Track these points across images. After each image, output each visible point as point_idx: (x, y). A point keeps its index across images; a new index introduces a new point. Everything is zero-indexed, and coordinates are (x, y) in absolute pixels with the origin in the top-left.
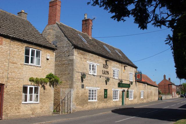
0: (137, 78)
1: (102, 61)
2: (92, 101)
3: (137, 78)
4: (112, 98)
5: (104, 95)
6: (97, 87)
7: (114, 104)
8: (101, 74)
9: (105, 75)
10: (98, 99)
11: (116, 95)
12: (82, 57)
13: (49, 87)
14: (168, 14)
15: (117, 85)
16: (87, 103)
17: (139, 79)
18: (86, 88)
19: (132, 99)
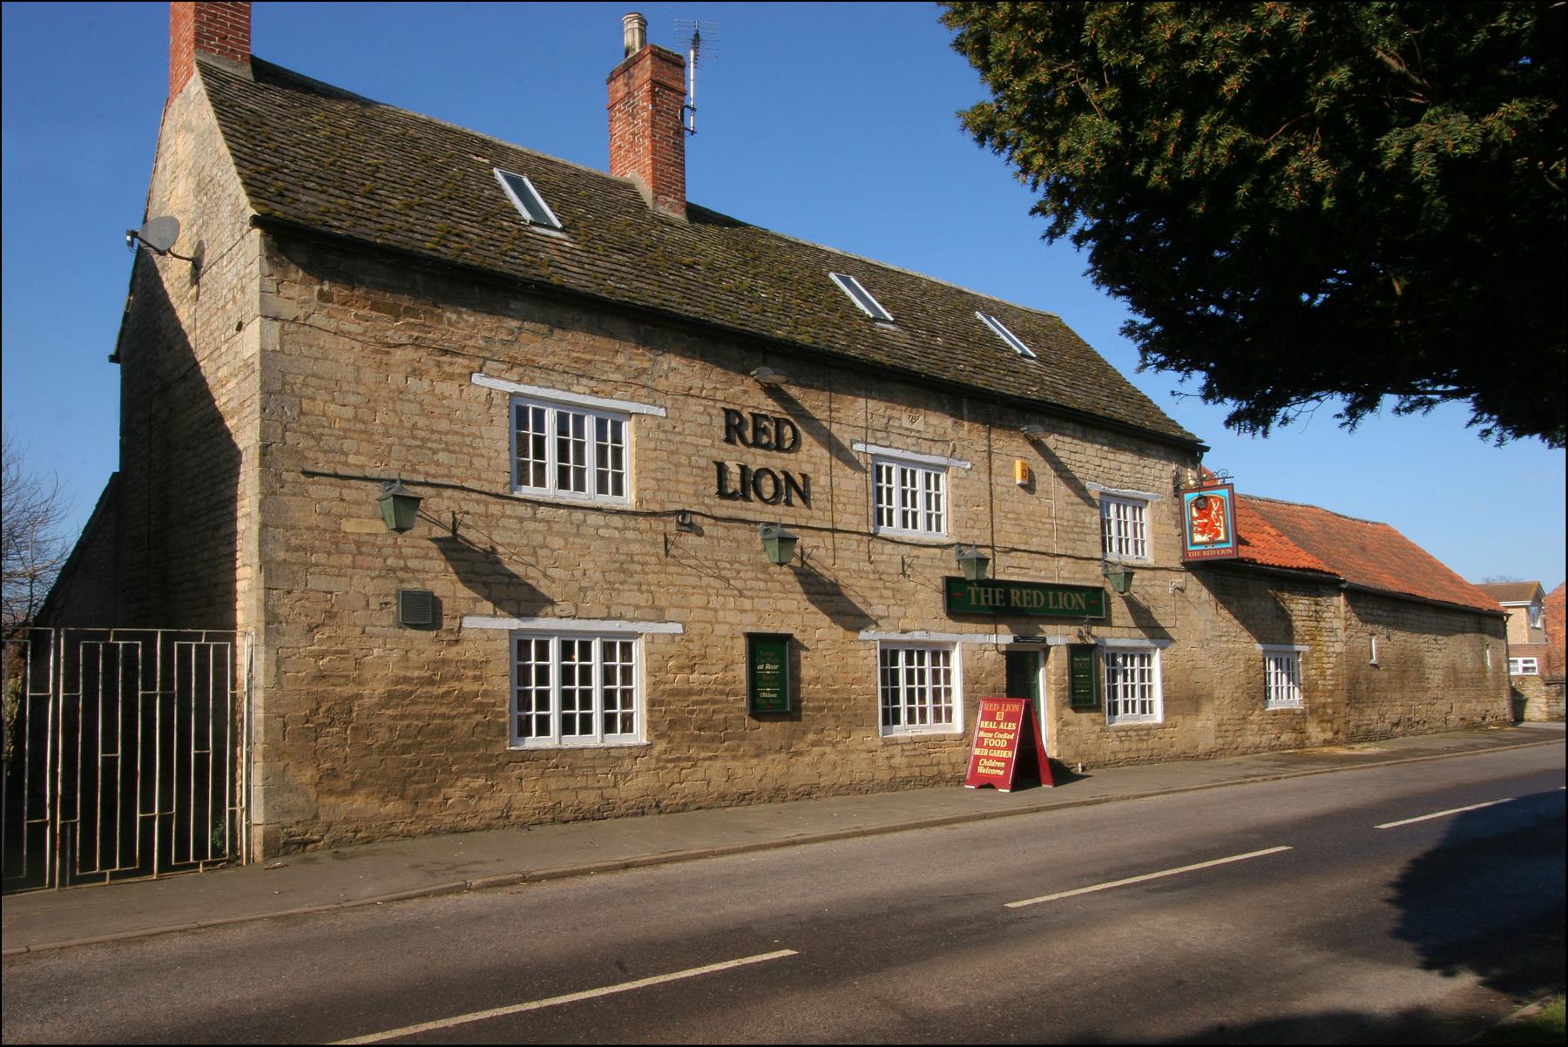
0: (1198, 538)
1: (697, 383)
2: (576, 740)
3: (1198, 538)
4: (870, 707)
5: (742, 685)
6: (630, 614)
7: (897, 761)
8: (694, 492)
9: (756, 504)
10: (652, 726)
11: (576, 661)
12: (392, 336)
13: (715, 778)
14: (17, 537)
15: (937, 602)
16: (497, 766)
17: (1212, 542)
18: (468, 622)
19: (1158, 716)
